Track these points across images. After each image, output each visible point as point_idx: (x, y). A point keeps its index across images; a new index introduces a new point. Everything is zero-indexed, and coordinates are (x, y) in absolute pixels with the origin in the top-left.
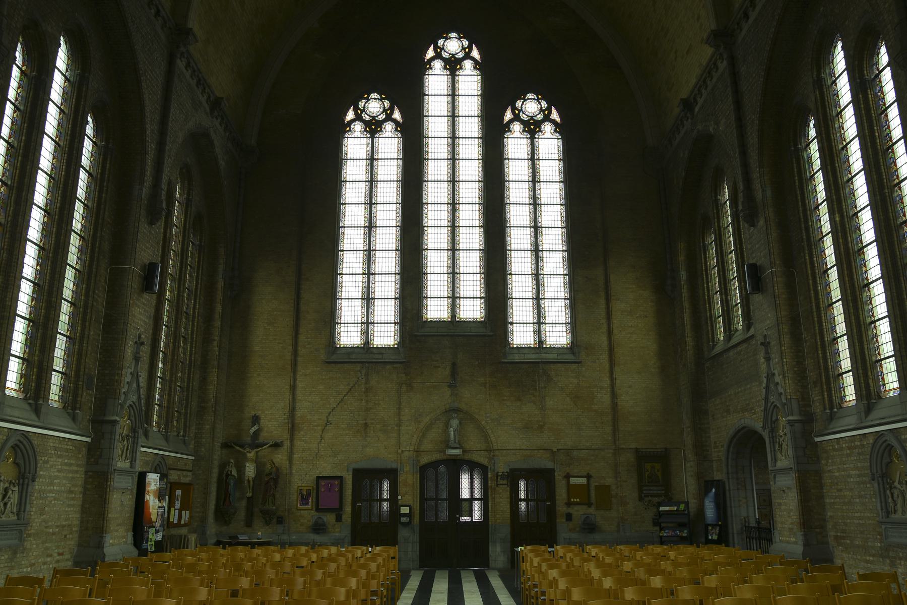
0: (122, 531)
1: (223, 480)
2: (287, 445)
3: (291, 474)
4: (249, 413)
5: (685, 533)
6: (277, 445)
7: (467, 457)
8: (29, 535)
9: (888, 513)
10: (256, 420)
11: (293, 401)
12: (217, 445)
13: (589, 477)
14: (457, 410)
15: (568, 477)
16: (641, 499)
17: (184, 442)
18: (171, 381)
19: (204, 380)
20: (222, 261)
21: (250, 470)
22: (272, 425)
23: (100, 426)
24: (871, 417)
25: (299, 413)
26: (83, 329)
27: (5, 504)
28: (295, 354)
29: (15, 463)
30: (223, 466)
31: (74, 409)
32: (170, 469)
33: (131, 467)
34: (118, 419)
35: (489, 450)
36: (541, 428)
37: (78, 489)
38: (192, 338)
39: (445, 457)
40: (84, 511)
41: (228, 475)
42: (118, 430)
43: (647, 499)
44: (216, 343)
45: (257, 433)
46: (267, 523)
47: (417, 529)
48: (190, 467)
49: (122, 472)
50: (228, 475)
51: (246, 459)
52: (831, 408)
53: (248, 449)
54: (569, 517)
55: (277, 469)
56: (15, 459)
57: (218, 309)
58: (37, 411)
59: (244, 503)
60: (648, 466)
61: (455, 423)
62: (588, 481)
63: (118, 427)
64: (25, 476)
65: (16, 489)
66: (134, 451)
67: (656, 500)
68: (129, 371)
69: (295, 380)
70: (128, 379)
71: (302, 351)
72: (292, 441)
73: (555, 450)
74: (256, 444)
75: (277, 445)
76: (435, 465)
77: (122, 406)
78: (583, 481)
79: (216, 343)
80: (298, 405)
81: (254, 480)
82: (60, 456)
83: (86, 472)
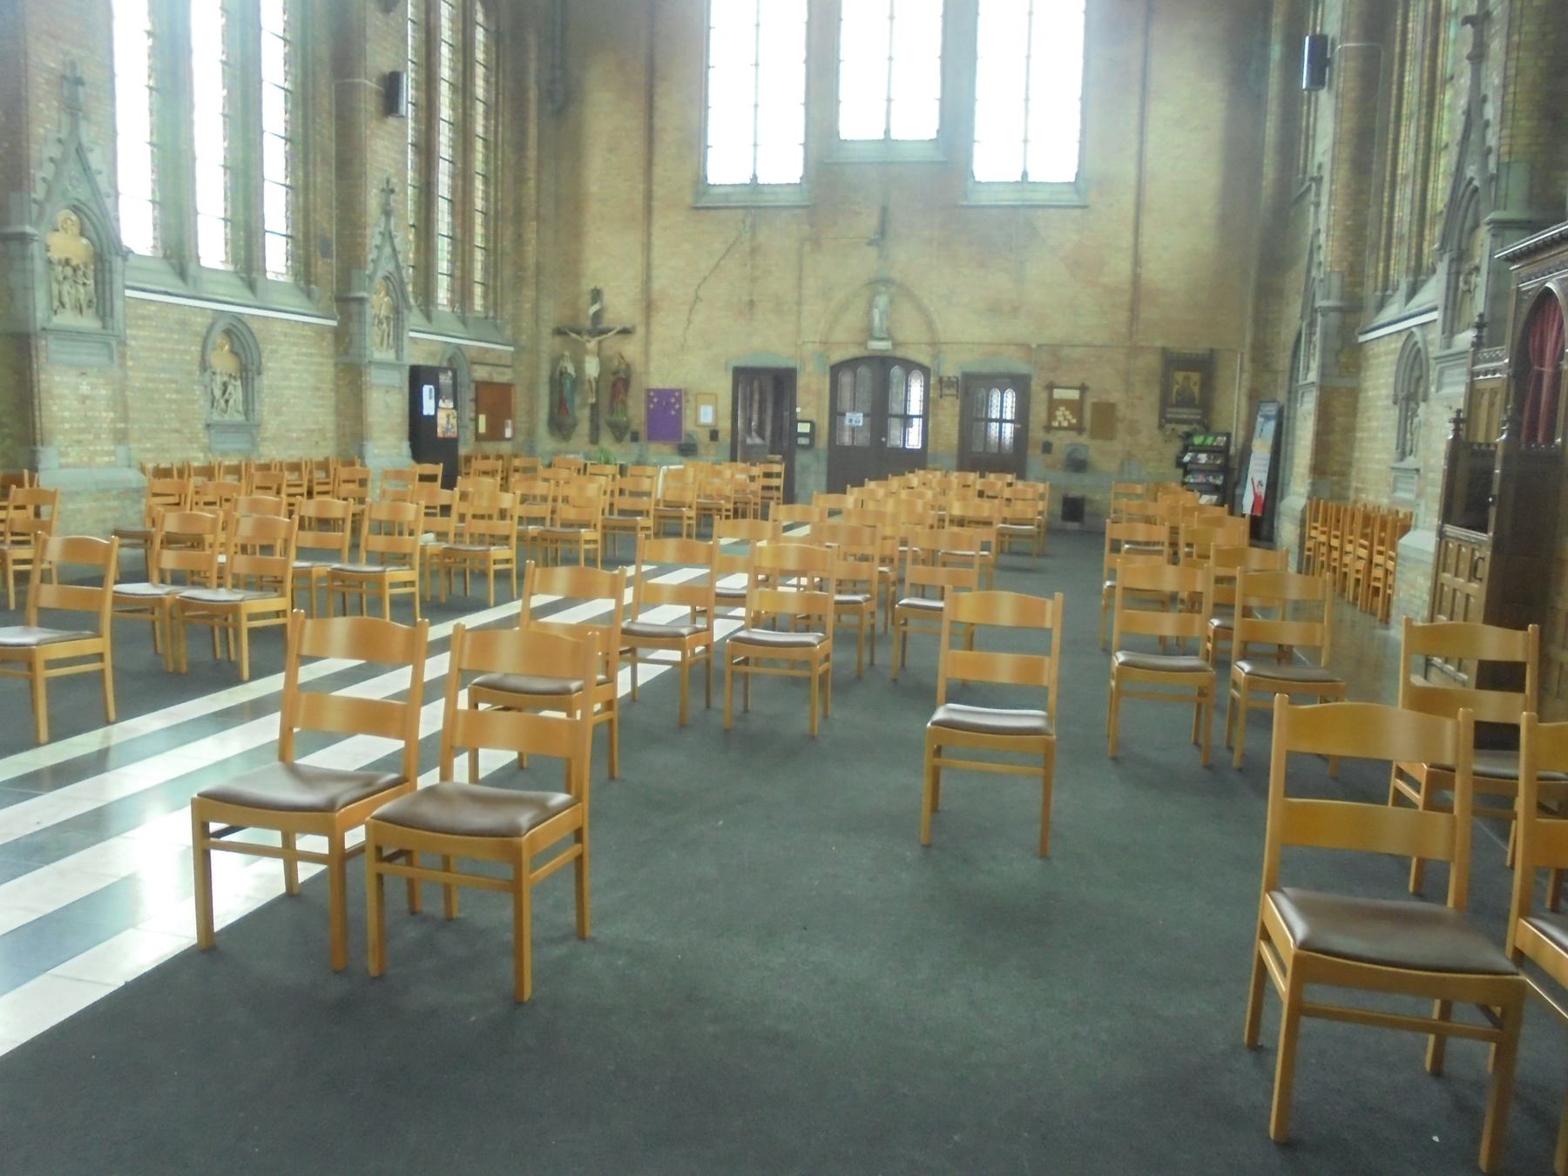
0: (391, 439)
1: (558, 381)
2: (640, 331)
3: (647, 373)
4: (587, 285)
5: (1219, 481)
6: (625, 332)
7: (900, 353)
8: (264, 439)
9: (1403, 455)
10: (596, 295)
11: (648, 267)
12: (546, 331)
13: (1083, 389)
14: (887, 282)
15: (1051, 387)
16: (1161, 427)
17: (496, 327)
18: (463, 241)
19: (519, 239)
20: (533, 55)
21: (592, 368)
22: (620, 306)
23: (346, 304)
24: (1412, 304)
25: (656, 286)
26: (306, 175)
27: (227, 402)
28: (649, 196)
29: (233, 352)
30: (556, 360)
31: (308, 282)
32: (474, 363)
33: (398, 358)
34: (365, 295)
35: (934, 344)
36: (1015, 311)
37: (328, 386)
38: (496, 178)
39: (866, 353)
40: (339, 413)
41: (562, 374)
42: (370, 311)
43: (1169, 426)
44: (532, 184)
45: (597, 316)
46: (619, 439)
47: (824, 455)
48: (508, 361)
49: (383, 365)
50: (562, 374)
51: (586, 352)
52: (1385, 289)
53: (586, 337)
54: (1047, 448)
55: (628, 366)
56: (232, 345)
57: (533, 131)
58: (251, 286)
59: (586, 412)
60: (1179, 376)
61: (882, 301)
62: (1082, 396)
63: (368, 306)
64: (248, 370)
65: (239, 383)
66: (398, 338)
67: (1185, 428)
68: (378, 230)
69: (649, 235)
70: (377, 240)
71: (659, 191)
72: (648, 324)
73: (1034, 346)
74: (598, 331)
75: (625, 332)
76: (851, 364)
77: (371, 278)
78: (1074, 395)
79: (532, 184)
80: (655, 273)
81: (597, 381)
82: (295, 344)
83: (336, 365)
